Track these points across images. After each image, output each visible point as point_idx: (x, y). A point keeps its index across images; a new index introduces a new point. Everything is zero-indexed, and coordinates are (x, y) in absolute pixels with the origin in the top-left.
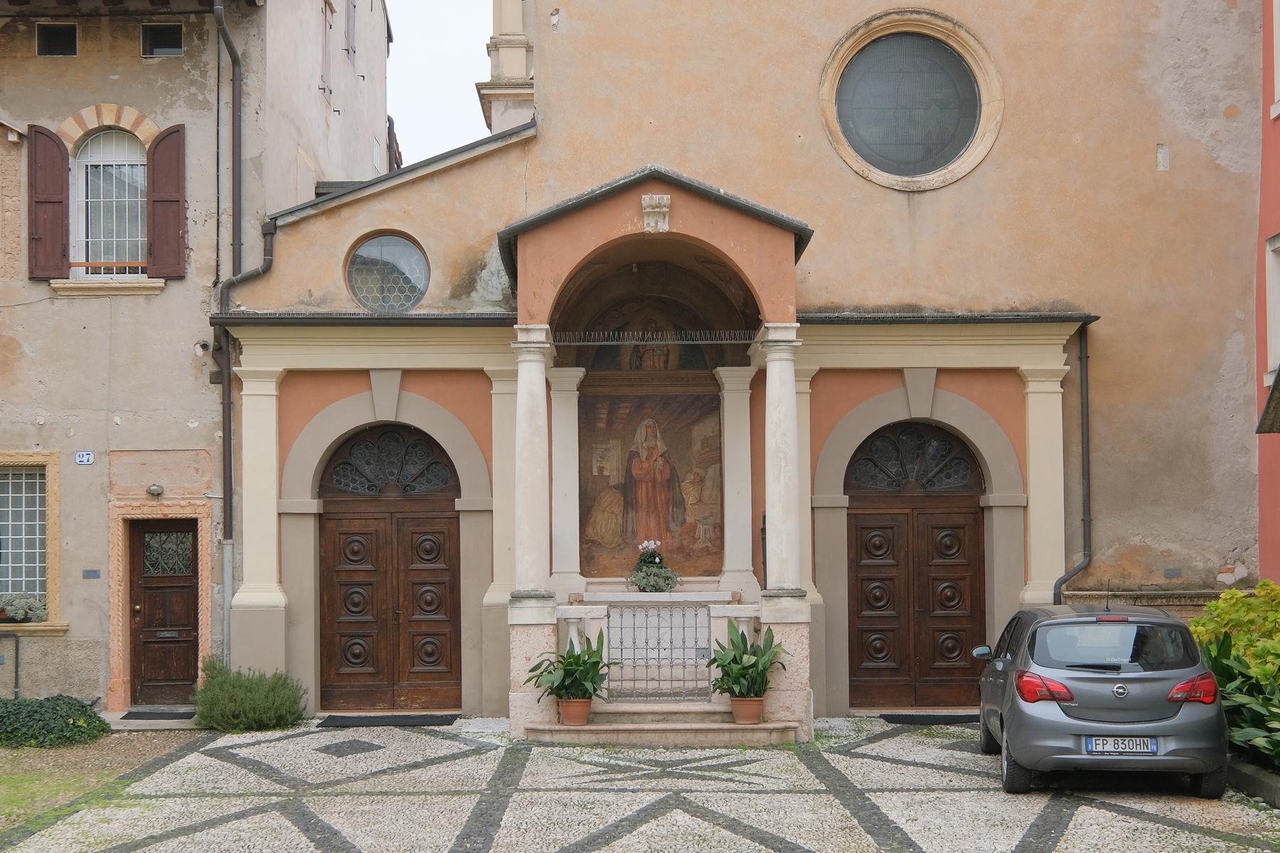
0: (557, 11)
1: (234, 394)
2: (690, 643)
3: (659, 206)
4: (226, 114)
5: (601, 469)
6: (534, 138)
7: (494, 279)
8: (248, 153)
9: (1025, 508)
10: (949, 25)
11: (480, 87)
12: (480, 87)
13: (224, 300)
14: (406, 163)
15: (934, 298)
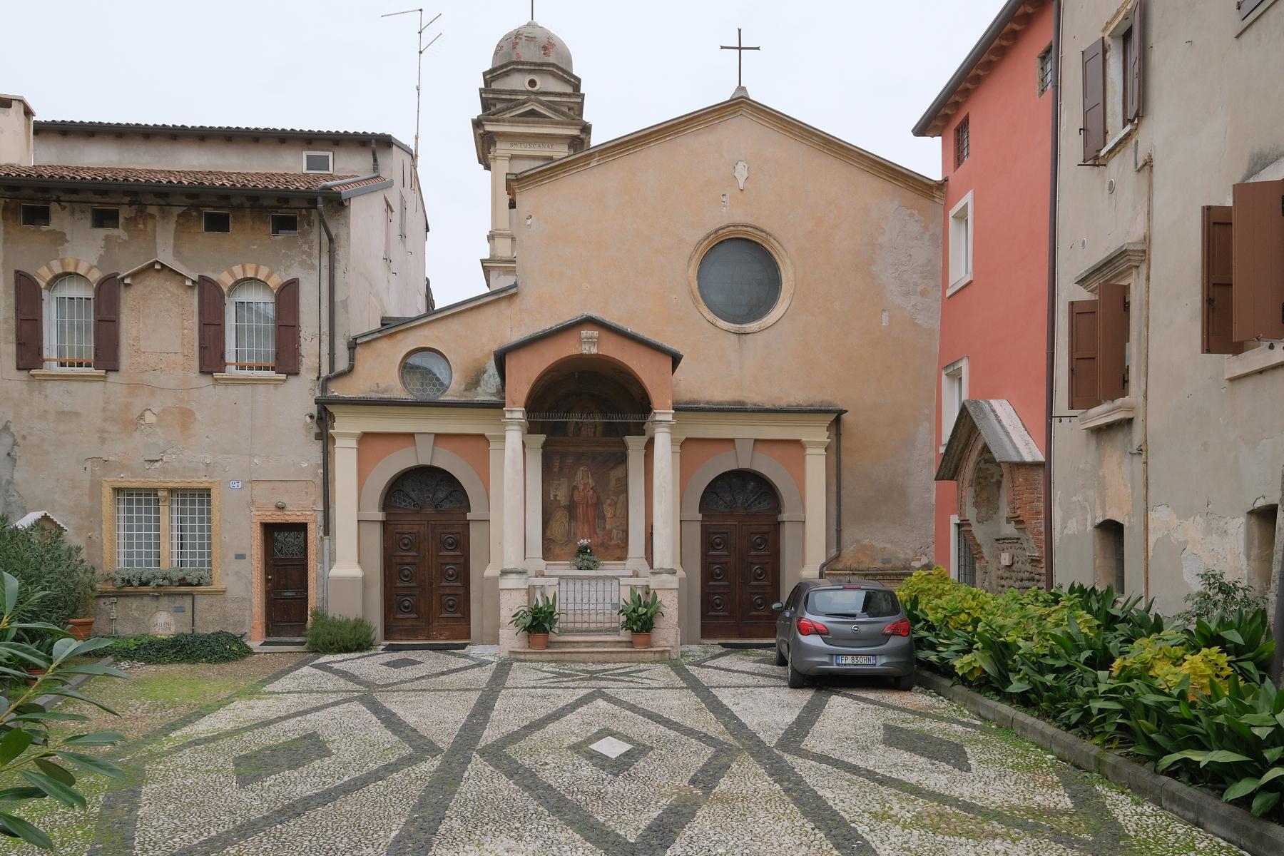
2: (608, 600)
5: (555, 496)
6: (512, 296)
7: (491, 379)
8: (339, 297)
11: (483, 261)
12: (483, 261)
13: (324, 388)
15: (753, 396)
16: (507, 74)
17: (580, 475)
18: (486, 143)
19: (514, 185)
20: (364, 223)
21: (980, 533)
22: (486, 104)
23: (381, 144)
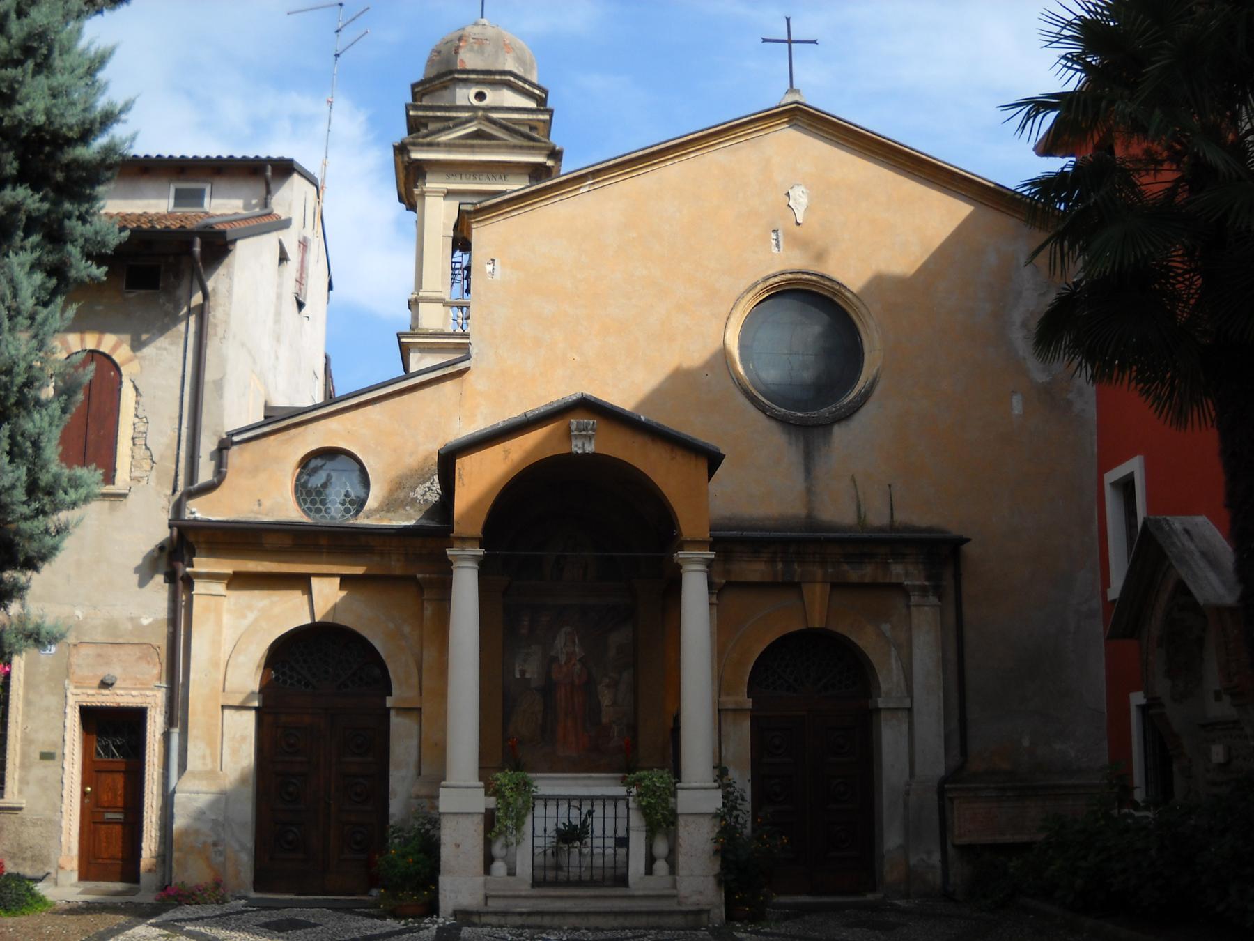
0: (493, 260)
2: (610, 832)
3: (585, 429)
5: (523, 672)
8: (209, 375)
9: (910, 710)
11: (399, 336)
14: (338, 393)
17: (560, 641)
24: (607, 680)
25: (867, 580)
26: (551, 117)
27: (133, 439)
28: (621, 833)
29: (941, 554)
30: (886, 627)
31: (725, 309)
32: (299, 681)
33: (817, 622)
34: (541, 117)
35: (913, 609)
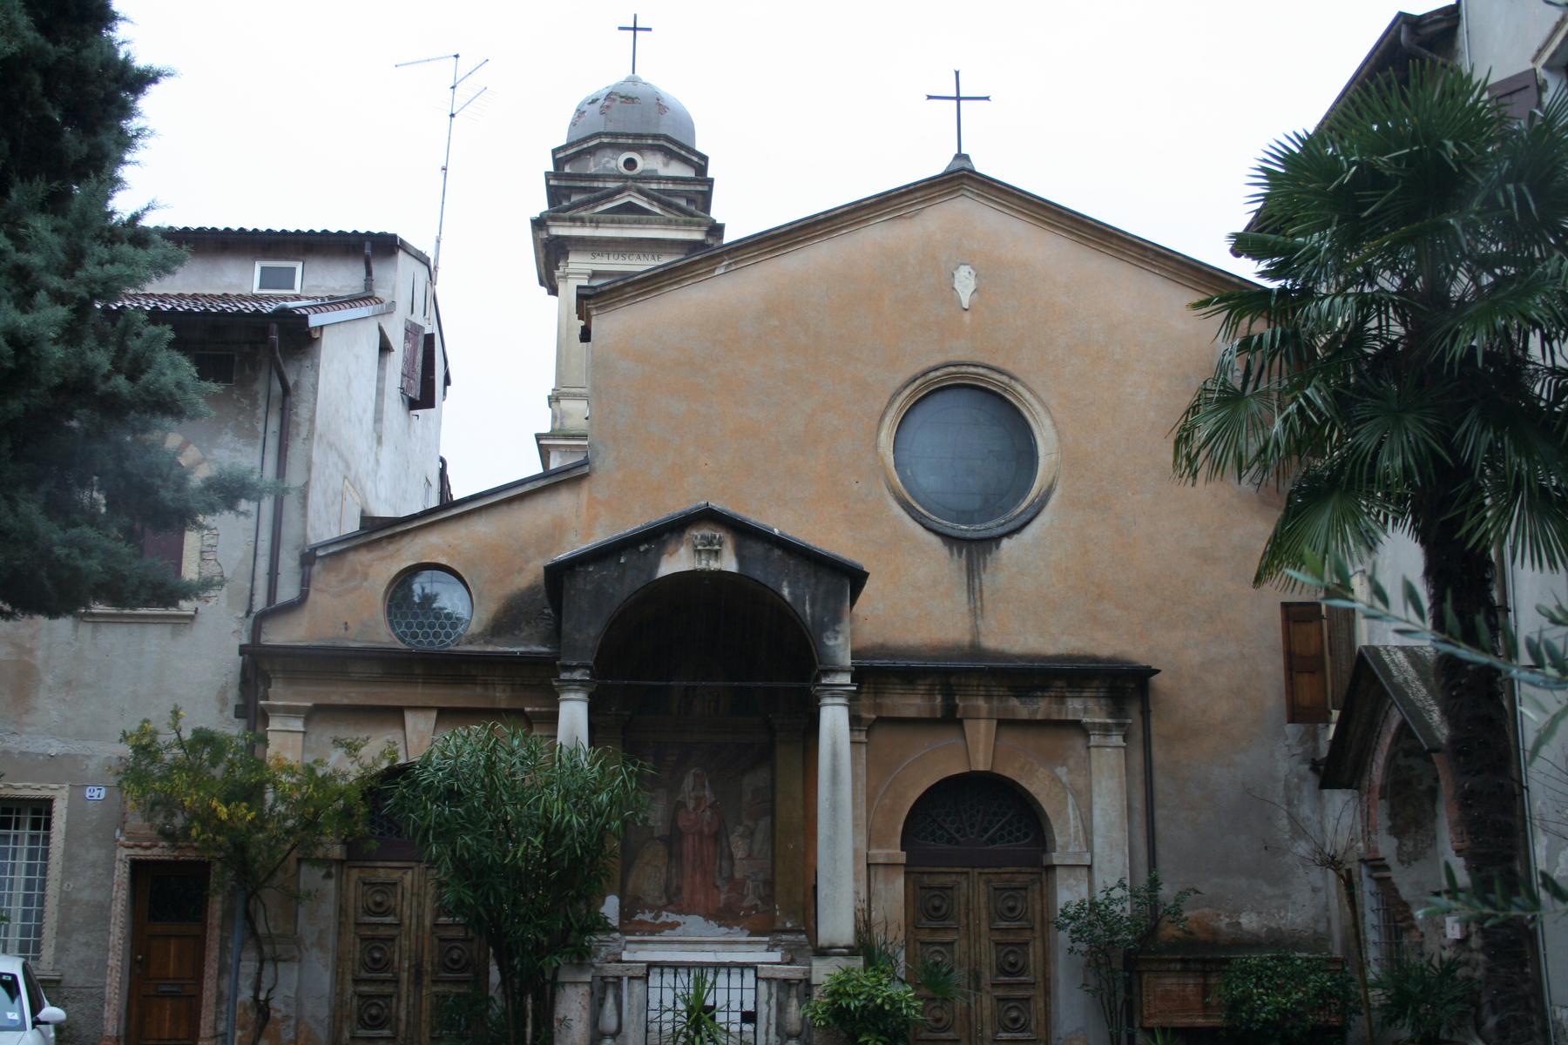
1: (1143, 879)
2: (735, 1006)
4: (272, 443)
5: (646, 819)
6: (586, 475)
9: (1090, 867)
10: (1005, 379)
11: (539, 437)
12: (539, 437)
13: (256, 631)
14: (457, 494)
16: (591, 151)
17: (689, 782)
18: (552, 256)
19: (590, 301)
20: (347, 372)
21: (1405, 881)
22: (554, 195)
23: (385, 246)
24: (741, 829)
25: (1039, 717)
26: (711, 187)
27: (202, 552)
28: (749, 1007)
29: (1126, 686)
30: (1061, 771)
31: (879, 406)
32: (390, 830)
33: (981, 763)
34: (699, 188)
35: (1093, 750)
